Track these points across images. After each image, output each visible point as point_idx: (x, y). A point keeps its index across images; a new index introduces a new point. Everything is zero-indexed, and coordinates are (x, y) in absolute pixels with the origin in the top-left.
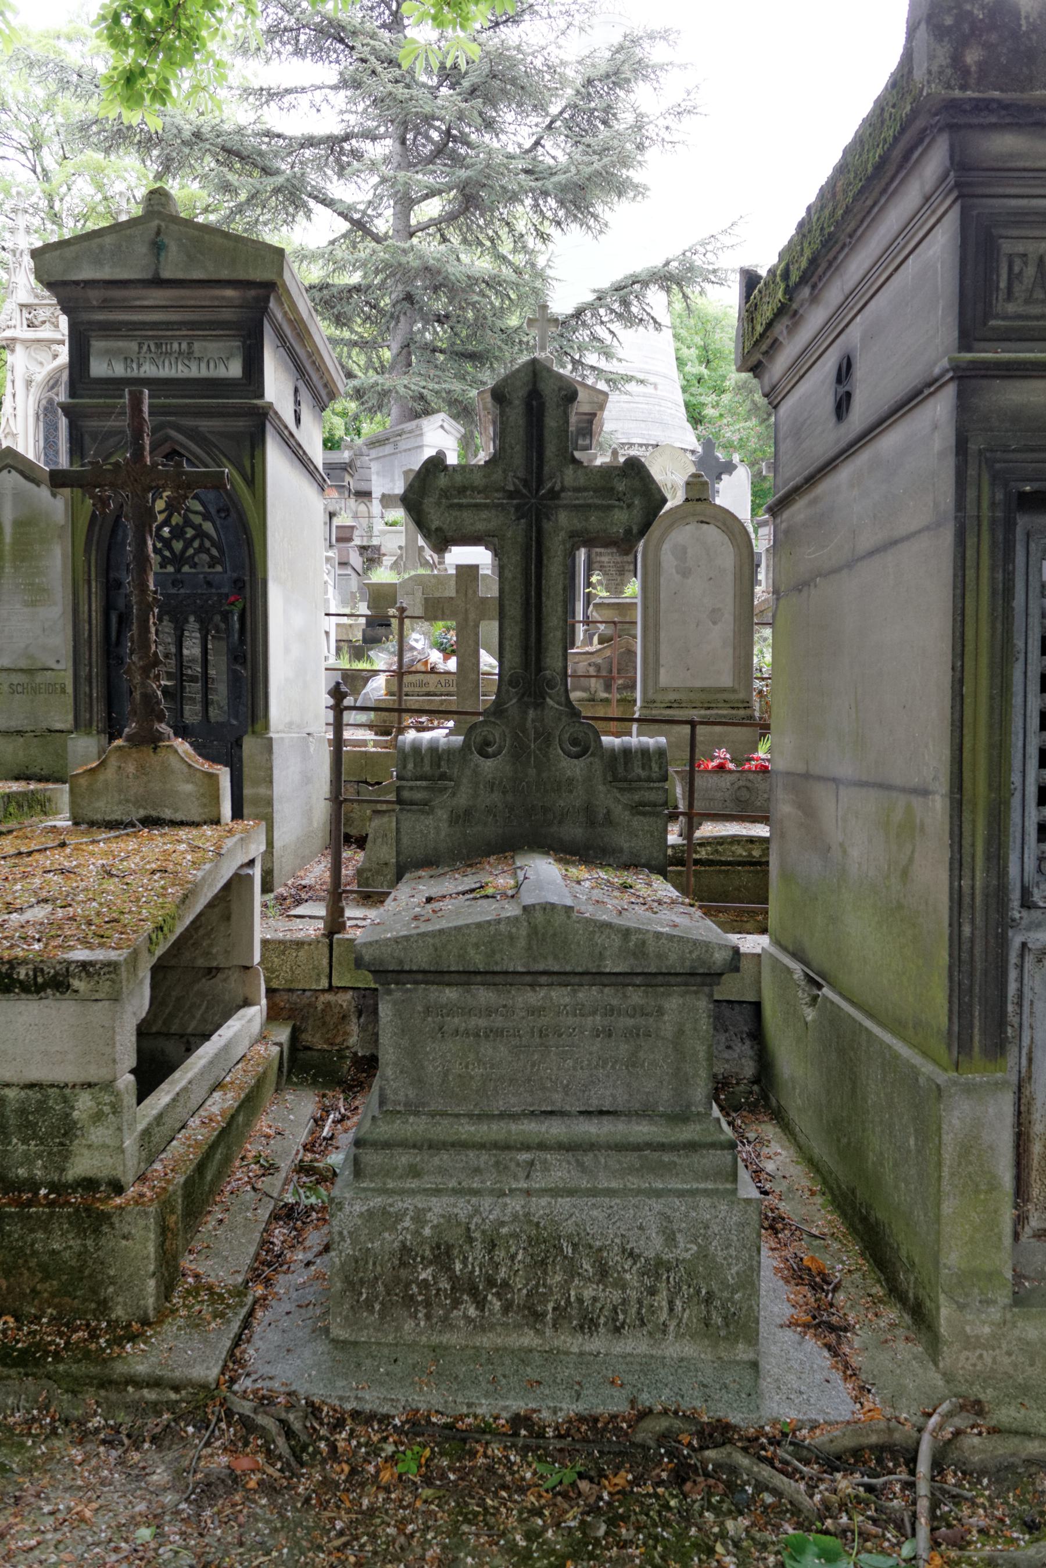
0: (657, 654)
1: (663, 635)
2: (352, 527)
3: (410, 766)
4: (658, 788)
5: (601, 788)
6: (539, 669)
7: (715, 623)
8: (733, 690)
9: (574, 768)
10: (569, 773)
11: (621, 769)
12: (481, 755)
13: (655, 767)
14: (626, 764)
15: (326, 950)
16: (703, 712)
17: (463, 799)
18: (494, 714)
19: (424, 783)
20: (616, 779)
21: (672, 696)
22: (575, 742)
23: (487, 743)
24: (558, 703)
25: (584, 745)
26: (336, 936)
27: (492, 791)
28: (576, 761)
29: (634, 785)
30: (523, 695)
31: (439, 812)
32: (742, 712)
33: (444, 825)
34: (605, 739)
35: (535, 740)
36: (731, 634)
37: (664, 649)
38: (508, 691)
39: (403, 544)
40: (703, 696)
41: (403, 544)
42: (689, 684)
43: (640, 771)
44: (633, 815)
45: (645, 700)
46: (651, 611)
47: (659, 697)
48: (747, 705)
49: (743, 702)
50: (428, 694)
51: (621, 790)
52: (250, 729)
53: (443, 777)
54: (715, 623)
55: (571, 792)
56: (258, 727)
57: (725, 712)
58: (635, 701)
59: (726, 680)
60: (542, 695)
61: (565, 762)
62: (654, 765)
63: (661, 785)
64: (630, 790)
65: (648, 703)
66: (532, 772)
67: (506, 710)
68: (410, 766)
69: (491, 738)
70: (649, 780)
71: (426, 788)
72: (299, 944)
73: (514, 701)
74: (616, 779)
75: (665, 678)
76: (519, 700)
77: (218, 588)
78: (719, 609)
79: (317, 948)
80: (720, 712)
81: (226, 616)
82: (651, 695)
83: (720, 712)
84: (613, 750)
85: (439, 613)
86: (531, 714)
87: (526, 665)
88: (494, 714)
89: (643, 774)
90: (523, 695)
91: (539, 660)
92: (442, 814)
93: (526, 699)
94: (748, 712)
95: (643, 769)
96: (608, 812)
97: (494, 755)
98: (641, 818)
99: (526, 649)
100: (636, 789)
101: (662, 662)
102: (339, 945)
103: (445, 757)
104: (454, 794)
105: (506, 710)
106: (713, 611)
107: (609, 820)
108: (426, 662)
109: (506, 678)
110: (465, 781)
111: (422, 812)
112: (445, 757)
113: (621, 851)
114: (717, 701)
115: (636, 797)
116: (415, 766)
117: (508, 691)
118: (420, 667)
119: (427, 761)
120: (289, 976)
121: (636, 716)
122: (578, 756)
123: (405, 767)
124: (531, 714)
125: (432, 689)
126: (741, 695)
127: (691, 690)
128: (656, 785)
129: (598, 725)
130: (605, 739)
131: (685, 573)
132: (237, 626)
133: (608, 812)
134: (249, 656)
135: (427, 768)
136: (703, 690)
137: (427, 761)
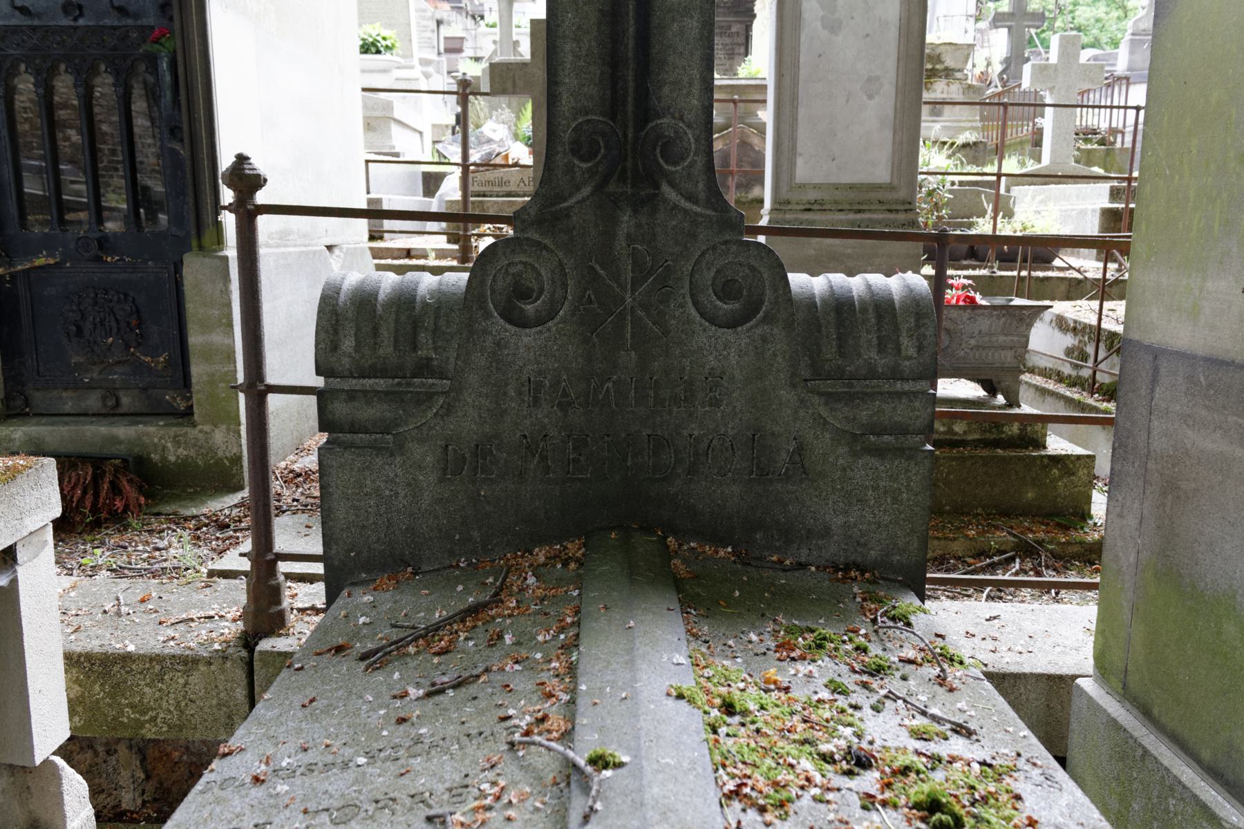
0: (793, 139)
1: (802, 113)
2: (462, 39)
3: (348, 344)
4: (915, 394)
5: (786, 394)
6: (645, 114)
7: (870, 97)
8: (890, 187)
9: (722, 351)
10: (712, 362)
11: (830, 352)
12: (510, 321)
13: (908, 346)
14: (841, 339)
15: (240, 674)
16: (851, 216)
17: (468, 422)
18: (539, 222)
19: (381, 384)
20: (818, 373)
21: (812, 195)
22: (727, 290)
23: (525, 294)
24: (691, 198)
25: (751, 292)
26: (265, 645)
27: (536, 402)
28: (728, 334)
29: (858, 387)
30: (605, 180)
31: (416, 451)
32: (902, 217)
33: (428, 479)
34: (797, 280)
35: (635, 284)
36: (891, 113)
37: (802, 133)
38: (570, 169)
39: (497, 38)
40: (852, 195)
41: (497, 38)
42: (833, 180)
43: (874, 354)
44: (855, 455)
45: (776, 200)
46: (787, 80)
47: (794, 197)
48: (908, 206)
49: (903, 203)
50: (509, 195)
51: (830, 398)
52: (194, 243)
53: (425, 368)
54: (870, 97)
55: (716, 403)
56: (207, 239)
57: (881, 216)
58: (761, 202)
59: (882, 174)
60: (650, 178)
61: (705, 337)
62: (905, 341)
63: (922, 385)
64: (850, 398)
65: (780, 204)
66: (628, 358)
67: (567, 214)
68: (348, 344)
69: (530, 282)
70: (895, 374)
71: (386, 395)
72: (188, 662)
73: (586, 191)
74: (818, 373)
75: (803, 171)
76: (599, 189)
77: (136, 16)
78: (877, 78)
79: (223, 671)
80: (875, 216)
81: (152, 60)
82: (785, 195)
83: (875, 216)
84: (812, 297)
85: (509, 85)
86: (626, 220)
87: (613, 108)
88: (539, 222)
89: (882, 362)
90: (605, 180)
91: (643, 94)
92: (424, 454)
93: (612, 188)
94: (910, 216)
95: (881, 348)
96: (800, 449)
97: (540, 321)
98: (873, 461)
99: (613, 62)
100: (866, 396)
101: (799, 150)
102: (265, 664)
103: (429, 322)
104: (448, 410)
105: (567, 214)
106: (869, 80)
107: (800, 465)
108: (506, 157)
109: (566, 136)
110: (473, 378)
111: (377, 449)
112: (429, 322)
113: (826, 532)
114: (870, 202)
115: (864, 415)
116: (358, 348)
117: (570, 169)
118: (499, 161)
119: (386, 333)
120: (174, 718)
121: (764, 222)
122: (733, 323)
123: (335, 347)
124: (626, 220)
125: (513, 188)
126: (902, 194)
127: (837, 187)
128: (907, 387)
129: (782, 247)
130: (797, 280)
131: (833, 27)
132: (168, 78)
133: (800, 449)
134: (185, 127)
135: (386, 350)
136: (852, 187)
137: (386, 333)
